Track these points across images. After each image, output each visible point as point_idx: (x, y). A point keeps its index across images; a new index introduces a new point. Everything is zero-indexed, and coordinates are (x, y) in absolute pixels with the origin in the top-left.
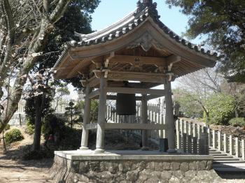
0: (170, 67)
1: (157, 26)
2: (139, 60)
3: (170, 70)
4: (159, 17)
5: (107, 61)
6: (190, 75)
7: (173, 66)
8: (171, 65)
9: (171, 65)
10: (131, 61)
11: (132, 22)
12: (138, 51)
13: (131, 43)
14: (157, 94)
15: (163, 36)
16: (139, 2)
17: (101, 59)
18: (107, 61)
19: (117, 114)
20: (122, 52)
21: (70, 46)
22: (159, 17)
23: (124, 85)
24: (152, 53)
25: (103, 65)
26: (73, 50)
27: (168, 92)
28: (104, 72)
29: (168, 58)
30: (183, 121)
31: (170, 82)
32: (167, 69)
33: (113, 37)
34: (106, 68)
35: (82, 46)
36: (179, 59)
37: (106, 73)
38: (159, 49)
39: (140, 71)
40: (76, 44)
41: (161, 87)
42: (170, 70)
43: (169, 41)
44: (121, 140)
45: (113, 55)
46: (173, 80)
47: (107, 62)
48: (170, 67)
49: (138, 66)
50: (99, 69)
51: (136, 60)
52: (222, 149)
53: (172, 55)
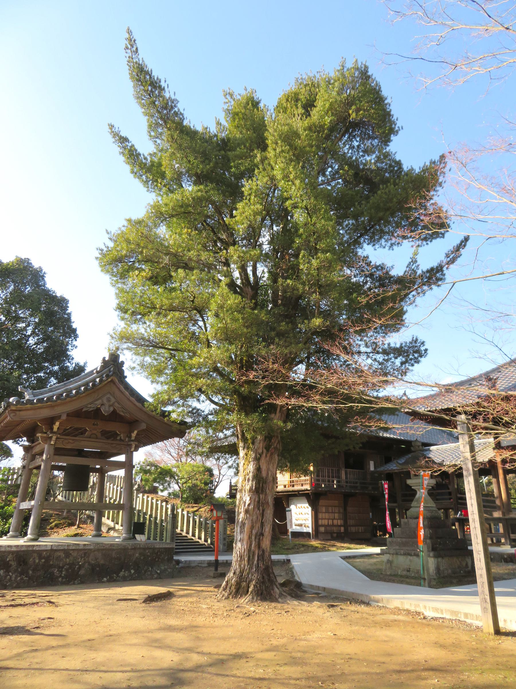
0: (134, 435)
1: (122, 387)
2: (97, 425)
3: (133, 438)
4: (126, 377)
5: (57, 424)
6: (160, 444)
7: (137, 434)
8: (136, 432)
9: (136, 432)
10: (87, 425)
11: (94, 381)
12: (96, 414)
13: (88, 404)
14: (119, 465)
15: (129, 399)
16: (104, 358)
17: (50, 421)
18: (57, 424)
19: (135, 508)
20: (78, 414)
21: (9, 404)
22: (126, 377)
23: (76, 453)
24: (114, 417)
25: (52, 429)
26: (13, 408)
27: (128, 465)
28: (51, 437)
29: (131, 423)
30: (152, 499)
31: (132, 453)
32: (130, 437)
33: (58, 398)
34: (55, 433)
35: (26, 404)
36: (143, 426)
37: (54, 438)
38: (122, 414)
39: (97, 438)
40: (18, 402)
41: (121, 458)
42: (133, 438)
43: (135, 405)
44: (124, 566)
45: (64, 417)
46: (136, 450)
47: (55, 428)
48: (134, 435)
49: (95, 432)
50: (46, 433)
51: (94, 424)
52: (188, 533)
53: (137, 421)
